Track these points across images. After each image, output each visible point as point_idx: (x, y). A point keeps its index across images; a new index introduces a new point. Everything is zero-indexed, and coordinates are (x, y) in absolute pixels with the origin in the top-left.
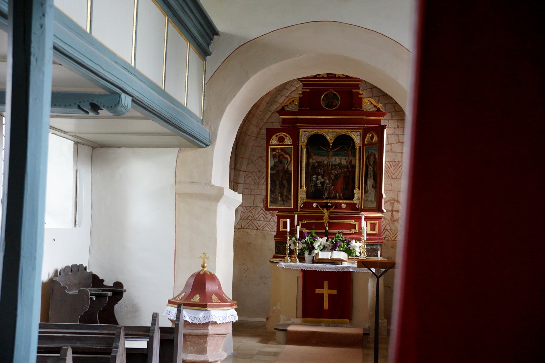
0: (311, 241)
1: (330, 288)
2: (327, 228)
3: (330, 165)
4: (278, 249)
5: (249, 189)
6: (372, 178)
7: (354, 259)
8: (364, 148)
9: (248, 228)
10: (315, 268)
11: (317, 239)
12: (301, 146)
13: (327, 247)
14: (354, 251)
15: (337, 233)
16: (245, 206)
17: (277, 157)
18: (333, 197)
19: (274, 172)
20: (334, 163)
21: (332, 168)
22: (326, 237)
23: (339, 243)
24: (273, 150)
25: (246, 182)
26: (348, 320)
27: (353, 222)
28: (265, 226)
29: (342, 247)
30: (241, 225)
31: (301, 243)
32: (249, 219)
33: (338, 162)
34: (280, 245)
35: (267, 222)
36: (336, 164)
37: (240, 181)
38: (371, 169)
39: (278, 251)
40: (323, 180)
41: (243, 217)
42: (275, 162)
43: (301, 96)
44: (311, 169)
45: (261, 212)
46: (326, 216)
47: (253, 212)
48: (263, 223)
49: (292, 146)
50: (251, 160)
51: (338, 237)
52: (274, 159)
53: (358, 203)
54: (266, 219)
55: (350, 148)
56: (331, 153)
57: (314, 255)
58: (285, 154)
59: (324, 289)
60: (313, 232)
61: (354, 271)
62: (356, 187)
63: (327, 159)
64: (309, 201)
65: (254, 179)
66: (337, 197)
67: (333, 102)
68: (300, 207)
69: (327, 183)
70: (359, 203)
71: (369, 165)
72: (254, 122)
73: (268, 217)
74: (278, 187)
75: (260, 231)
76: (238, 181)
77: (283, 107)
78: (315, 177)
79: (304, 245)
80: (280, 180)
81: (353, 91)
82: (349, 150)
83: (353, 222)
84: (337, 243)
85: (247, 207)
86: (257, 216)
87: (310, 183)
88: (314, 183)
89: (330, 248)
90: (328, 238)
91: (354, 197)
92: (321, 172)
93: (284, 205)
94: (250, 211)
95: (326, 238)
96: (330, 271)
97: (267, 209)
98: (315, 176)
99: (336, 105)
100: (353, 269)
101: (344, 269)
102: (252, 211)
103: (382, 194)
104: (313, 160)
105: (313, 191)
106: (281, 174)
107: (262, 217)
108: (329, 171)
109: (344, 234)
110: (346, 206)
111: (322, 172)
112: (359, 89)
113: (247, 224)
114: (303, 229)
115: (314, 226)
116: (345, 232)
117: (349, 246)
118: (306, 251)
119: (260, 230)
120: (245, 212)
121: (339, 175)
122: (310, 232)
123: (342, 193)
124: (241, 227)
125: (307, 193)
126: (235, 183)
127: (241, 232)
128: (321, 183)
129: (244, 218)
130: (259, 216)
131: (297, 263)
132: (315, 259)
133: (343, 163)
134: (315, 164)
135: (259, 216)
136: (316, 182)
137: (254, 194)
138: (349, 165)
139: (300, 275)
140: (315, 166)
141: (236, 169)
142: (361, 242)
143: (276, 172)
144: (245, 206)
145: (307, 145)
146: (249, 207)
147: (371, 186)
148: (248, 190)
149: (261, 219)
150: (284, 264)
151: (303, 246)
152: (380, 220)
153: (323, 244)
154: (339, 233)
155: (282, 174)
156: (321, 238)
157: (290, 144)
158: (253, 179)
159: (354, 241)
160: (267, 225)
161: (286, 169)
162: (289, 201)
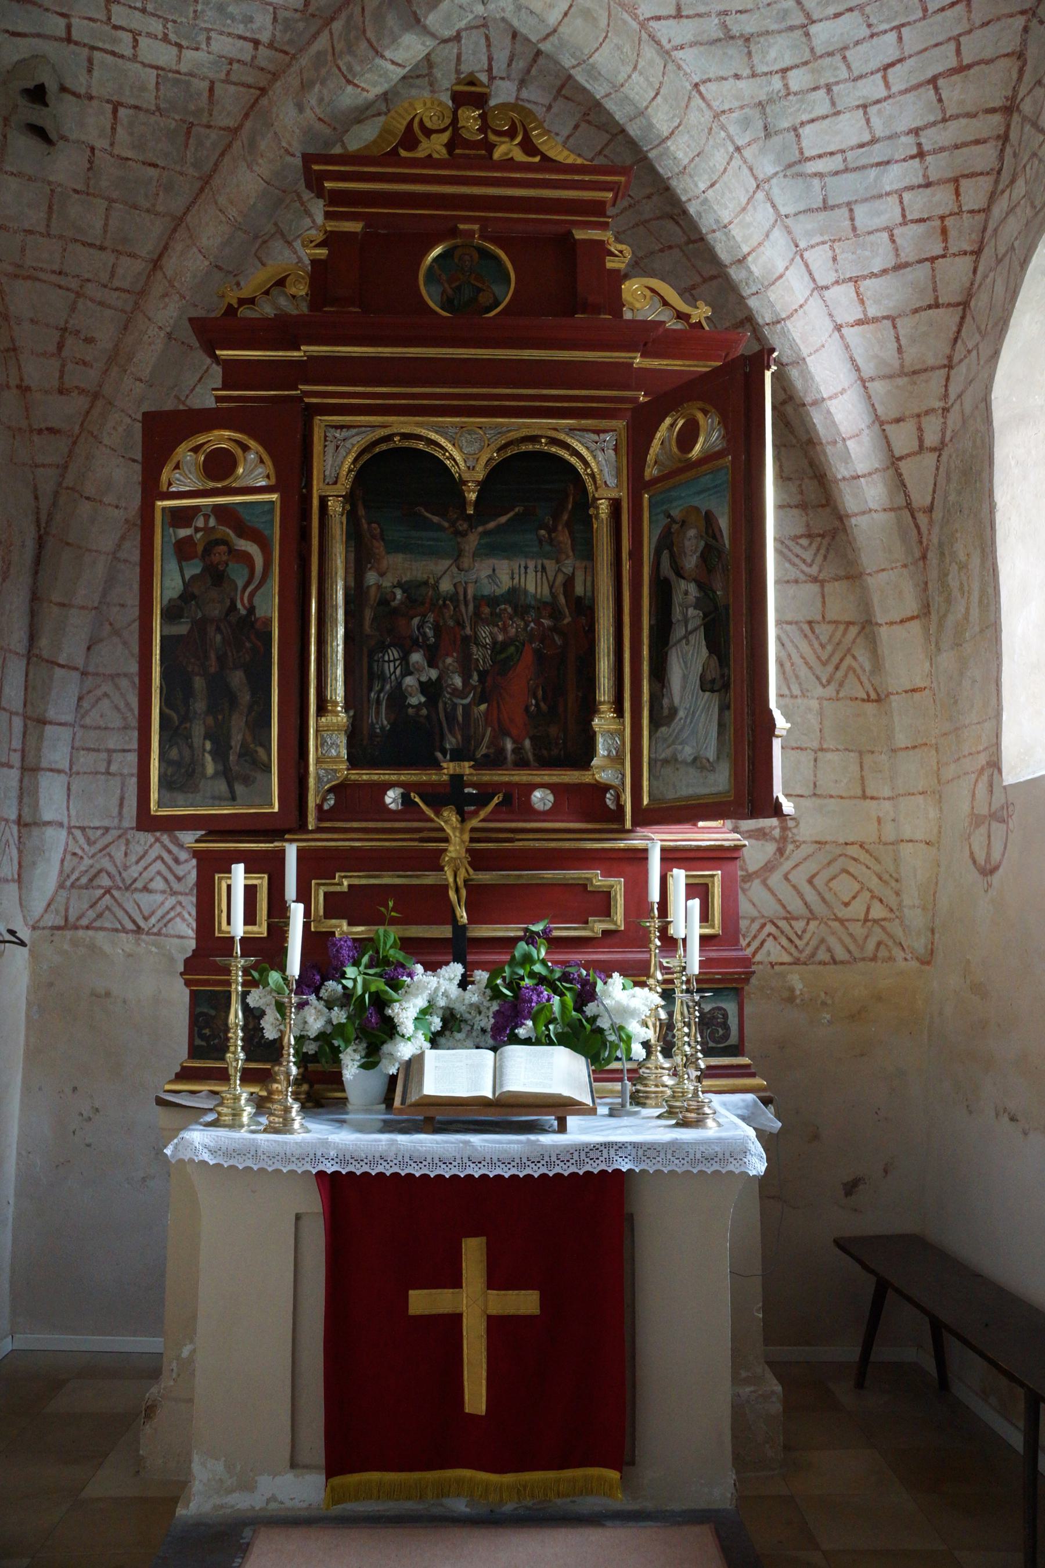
0: (373, 989)
1: (496, 1280)
2: (463, 915)
3: (470, 596)
4: (207, 1031)
5: (98, 750)
6: (699, 639)
7: (622, 1071)
8: (641, 498)
9: (97, 924)
10: (402, 1163)
11: (410, 975)
12: (323, 501)
13: (467, 1016)
14: (621, 1039)
15: (518, 939)
16: (83, 829)
17: (196, 557)
18: (485, 756)
19: (182, 629)
20: (488, 590)
21: (477, 613)
22: (456, 960)
23: (535, 998)
24: (180, 517)
25: (88, 721)
26: (614, 1475)
27: (598, 879)
28: (172, 914)
29: (557, 1015)
30: (63, 914)
31: (320, 1005)
32: (100, 887)
33: (505, 581)
34: (213, 1013)
35: (180, 898)
36: (499, 592)
37: (51, 714)
38: (686, 593)
39: (203, 1043)
40: (434, 674)
41: (73, 877)
42: (187, 577)
43: (323, 252)
44: (374, 619)
45: (153, 854)
46: (456, 848)
47: (118, 855)
48: (163, 903)
49: (274, 497)
50: (111, 624)
51: (528, 959)
52: (184, 563)
53: (616, 782)
54: (176, 886)
55: (565, 517)
56: (472, 541)
57: (393, 1071)
58: (241, 535)
59: (461, 1287)
60: (389, 935)
61: (643, 1166)
62: (603, 703)
63: (454, 569)
64: (365, 776)
65: (122, 705)
66: (505, 758)
67: (479, 290)
68: (319, 807)
69: (455, 689)
70: (623, 783)
71: (672, 576)
72: (110, 434)
73: (184, 876)
74: (200, 705)
75: (152, 937)
76: (45, 711)
77: (230, 305)
78: (395, 660)
79: (339, 1016)
80: (212, 670)
81: (577, 237)
82: (560, 528)
83: (598, 879)
84: (527, 994)
85: (90, 832)
86: (134, 871)
87: (370, 690)
88: (388, 687)
89: (488, 1022)
90: (469, 968)
91: (590, 750)
92: (424, 635)
93: (234, 798)
94: (107, 846)
95: (456, 970)
96: (499, 1177)
97: (146, 822)
98: (394, 653)
99: (497, 304)
100: (637, 1160)
101: (579, 1163)
102: (112, 849)
103: (771, 711)
104: (382, 575)
105: (382, 728)
106: (219, 637)
107: (159, 873)
108: (464, 628)
109: (556, 944)
110: (551, 798)
111: (430, 633)
112: (604, 226)
113: (91, 907)
114: (334, 922)
115: (391, 904)
116: (560, 931)
117: (591, 1009)
118: (349, 1050)
119: (148, 933)
120: (80, 853)
121: (512, 649)
122: (371, 940)
123: (532, 739)
124: (62, 923)
125: (353, 735)
126: (30, 718)
127: (66, 947)
128: (425, 687)
129: (78, 883)
130: (146, 868)
131: (291, 1132)
132: (403, 1102)
133: (531, 588)
134: (394, 594)
135: (146, 868)
136: (400, 684)
137: (121, 775)
138: (562, 599)
139: (313, 1203)
140: (393, 604)
141: (37, 656)
142: (651, 981)
143: (191, 631)
144: (83, 829)
145: (350, 498)
146: (99, 832)
147: (694, 680)
148: (95, 754)
149: (153, 885)
150: (207, 1141)
151: (329, 1021)
152: (730, 866)
153: (442, 1003)
154: (531, 938)
155: (223, 638)
156: (431, 967)
157: (263, 483)
158: (117, 708)
159: (617, 979)
160: (179, 909)
161: (243, 612)
162: (259, 776)
